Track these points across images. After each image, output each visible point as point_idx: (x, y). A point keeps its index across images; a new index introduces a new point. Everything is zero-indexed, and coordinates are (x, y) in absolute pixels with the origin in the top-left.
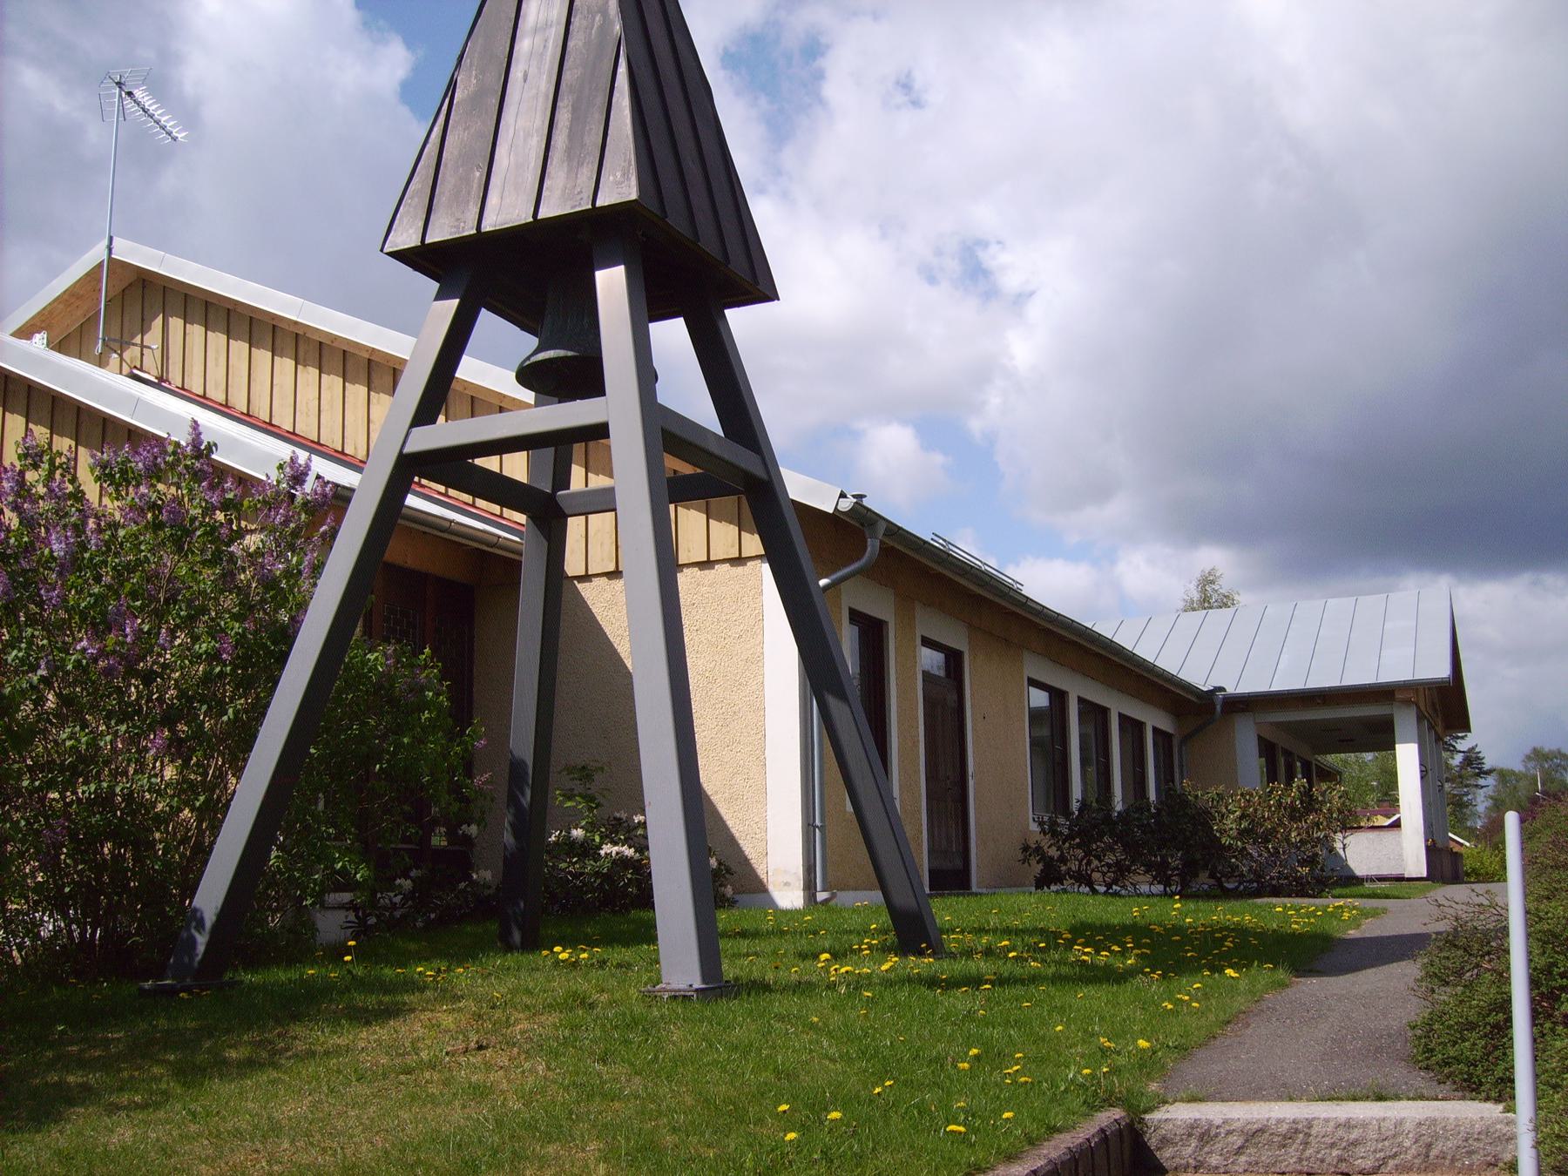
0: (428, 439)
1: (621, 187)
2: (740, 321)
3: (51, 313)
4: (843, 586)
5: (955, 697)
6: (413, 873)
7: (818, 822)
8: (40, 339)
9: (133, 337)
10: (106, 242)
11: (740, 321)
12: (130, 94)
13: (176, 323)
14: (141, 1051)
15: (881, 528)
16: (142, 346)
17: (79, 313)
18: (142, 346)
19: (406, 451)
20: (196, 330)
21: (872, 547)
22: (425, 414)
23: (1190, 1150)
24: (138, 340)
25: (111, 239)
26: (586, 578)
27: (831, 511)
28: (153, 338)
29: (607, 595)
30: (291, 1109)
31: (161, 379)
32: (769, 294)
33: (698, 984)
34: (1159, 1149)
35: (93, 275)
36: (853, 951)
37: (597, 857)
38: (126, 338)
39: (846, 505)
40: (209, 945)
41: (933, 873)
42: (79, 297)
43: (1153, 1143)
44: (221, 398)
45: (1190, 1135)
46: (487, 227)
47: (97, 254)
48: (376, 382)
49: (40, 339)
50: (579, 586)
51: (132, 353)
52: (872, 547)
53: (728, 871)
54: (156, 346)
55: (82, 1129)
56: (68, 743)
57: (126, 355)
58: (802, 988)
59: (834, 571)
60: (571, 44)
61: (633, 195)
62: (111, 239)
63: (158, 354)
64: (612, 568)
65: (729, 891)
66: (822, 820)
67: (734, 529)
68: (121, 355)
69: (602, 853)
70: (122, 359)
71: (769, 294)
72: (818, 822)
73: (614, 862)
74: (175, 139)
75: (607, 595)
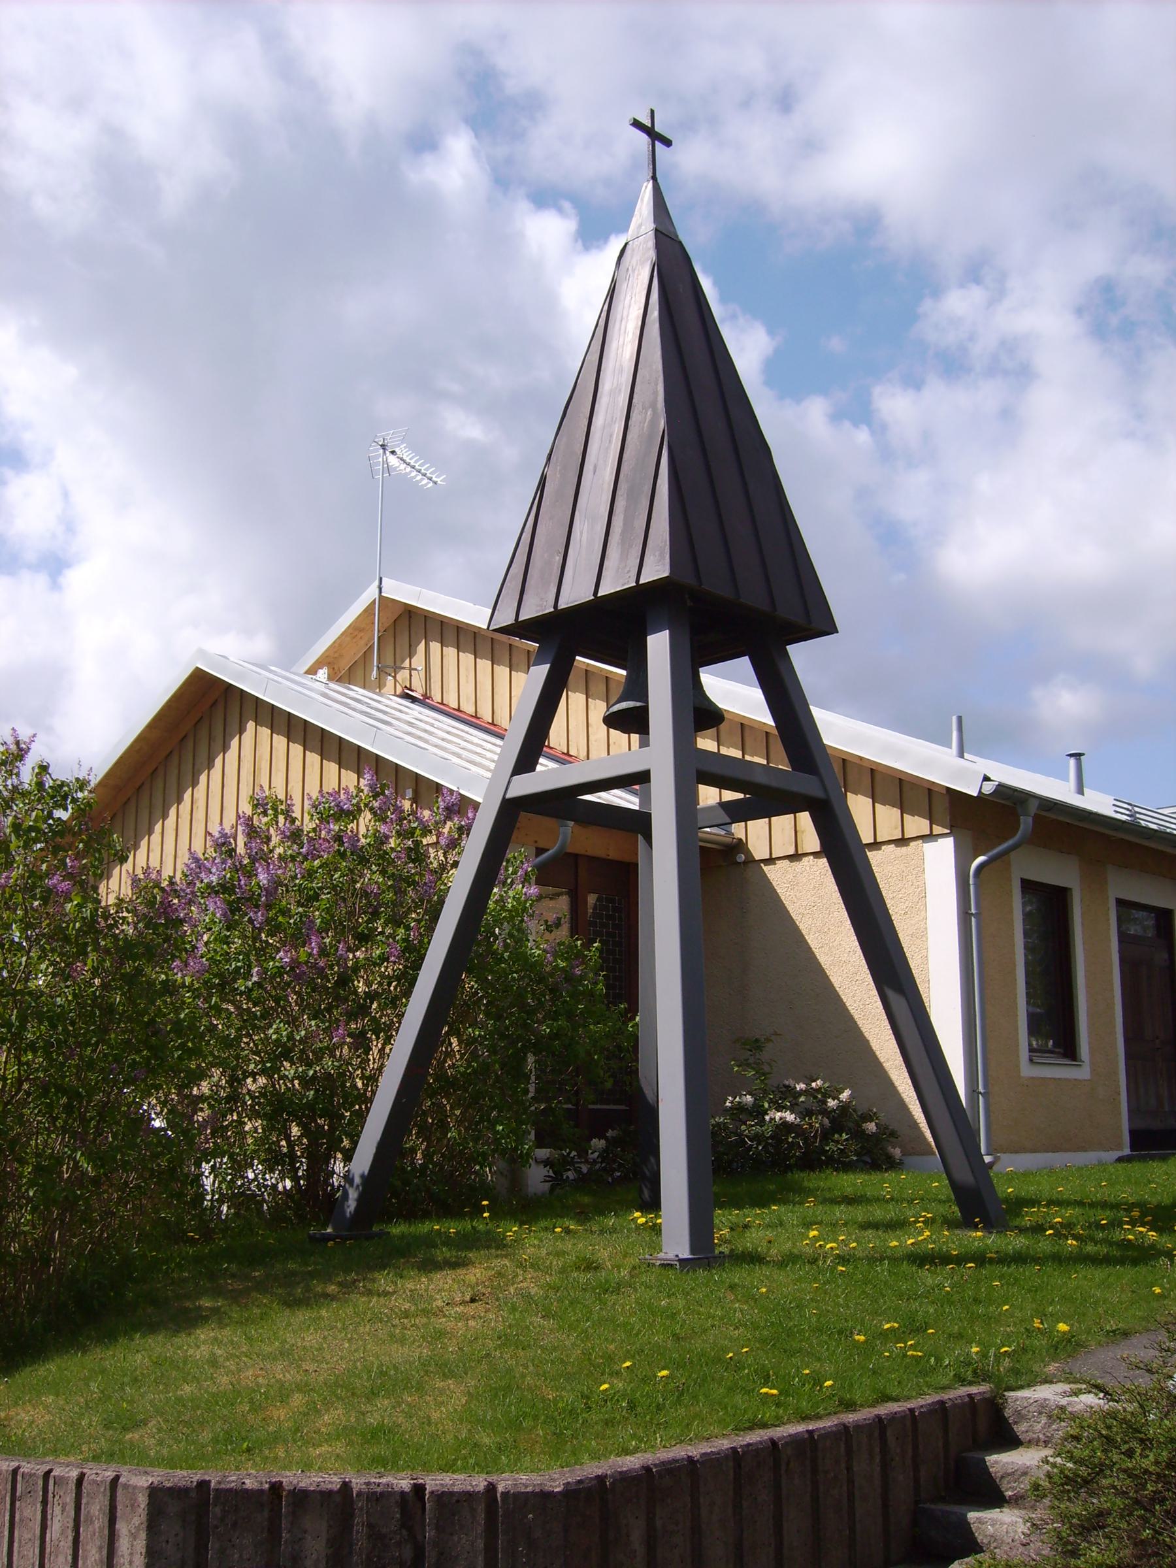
0: (525, 785)
1: (657, 569)
2: (801, 655)
3: (340, 645)
4: (1013, 854)
5: (1166, 956)
6: (610, 1133)
7: (981, 1089)
8: (323, 674)
9: (403, 661)
10: (377, 583)
11: (801, 655)
12: (393, 452)
13: (435, 646)
14: (261, 1287)
15: (1033, 807)
16: (411, 669)
17: (362, 642)
18: (411, 669)
19: (508, 796)
20: (451, 652)
21: (1026, 823)
22: (525, 762)
23: (1038, 1427)
24: (406, 664)
25: (381, 579)
26: (771, 861)
27: (975, 794)
28: (418, 661)
29: (790, 877)
30: (311, 1339)
31: (426, 696)
32: (827, 627)
33: (686, 1254)
34: (1016, 1423)
35: (369, 610)
36: (910, 1224)
37: (762, 1122)
38: (398, 664)
39: (988, 788)
40: (360, 1200)
41: (1132, 1133)
42: (361, 630)
43: (1008, 1413)
44: (471, 711)
45: (1040, 1413)
46: (562, 605)
47: (371, 594)
48: (592, 689)
49: (323, 674)
50: (765, 868)
51: (403, 675)
52: (1026, 823)
53: (893, 1134)
54: (421, 667)
55: (201, 1344)
56: (274, 1037)
57: (398, 677)
58: (789, 1260)
59: (992, 848)
60: (629, 438)
61: (666, 574)
62: (381, 579)
63: (423, 674)
64: (792, 851)
65: (897, 1152)
66: (985, 1086)
67: (896, 812)
68: (395, 677)
69: (767, 1118)
70: (396, 680)
71: (827, 627)
72: (981, 1089)
73: (777, 1126)
74: (435, 483)
75: (790, 877)
